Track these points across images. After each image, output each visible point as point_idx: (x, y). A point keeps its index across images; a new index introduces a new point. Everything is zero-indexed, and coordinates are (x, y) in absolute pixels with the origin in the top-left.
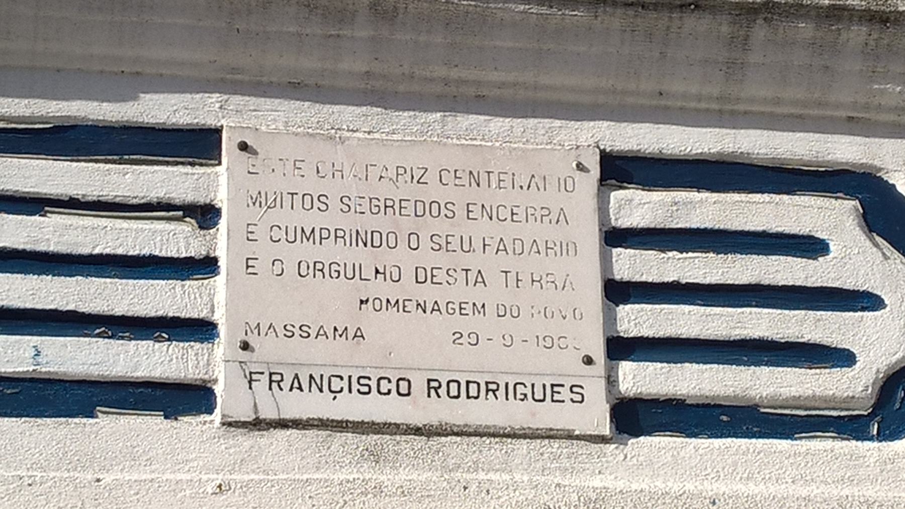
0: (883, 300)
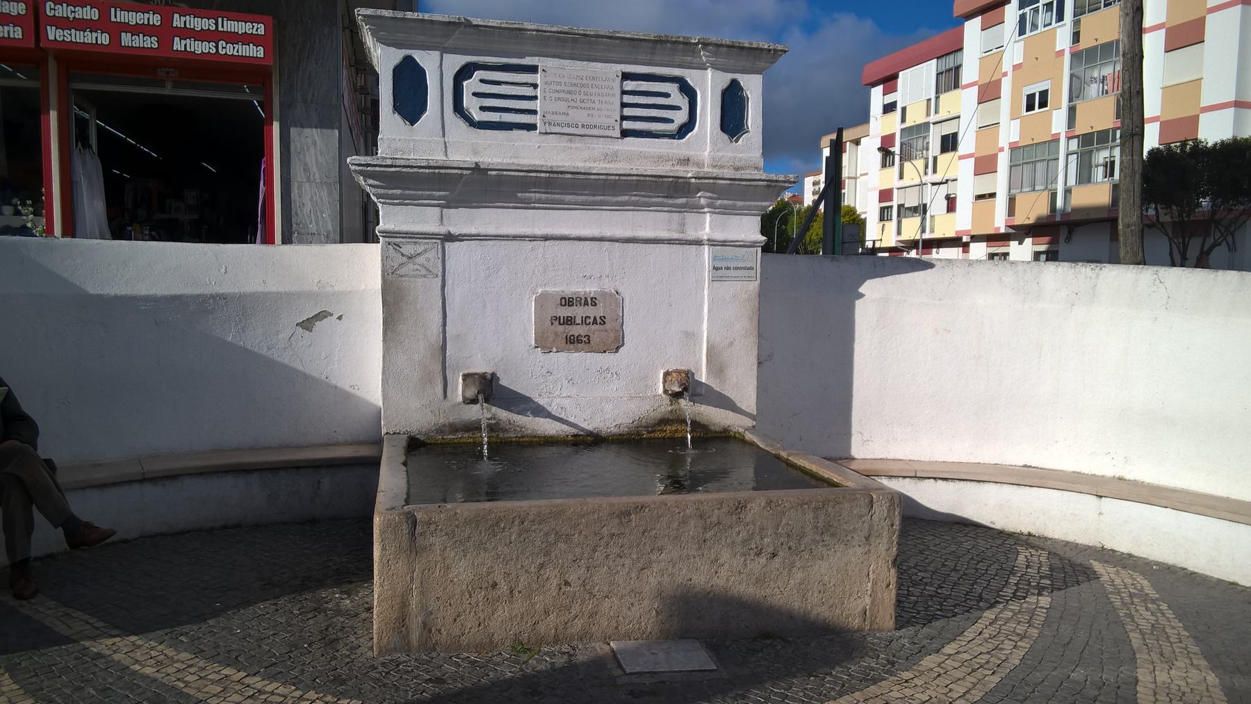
0: (423, 108)
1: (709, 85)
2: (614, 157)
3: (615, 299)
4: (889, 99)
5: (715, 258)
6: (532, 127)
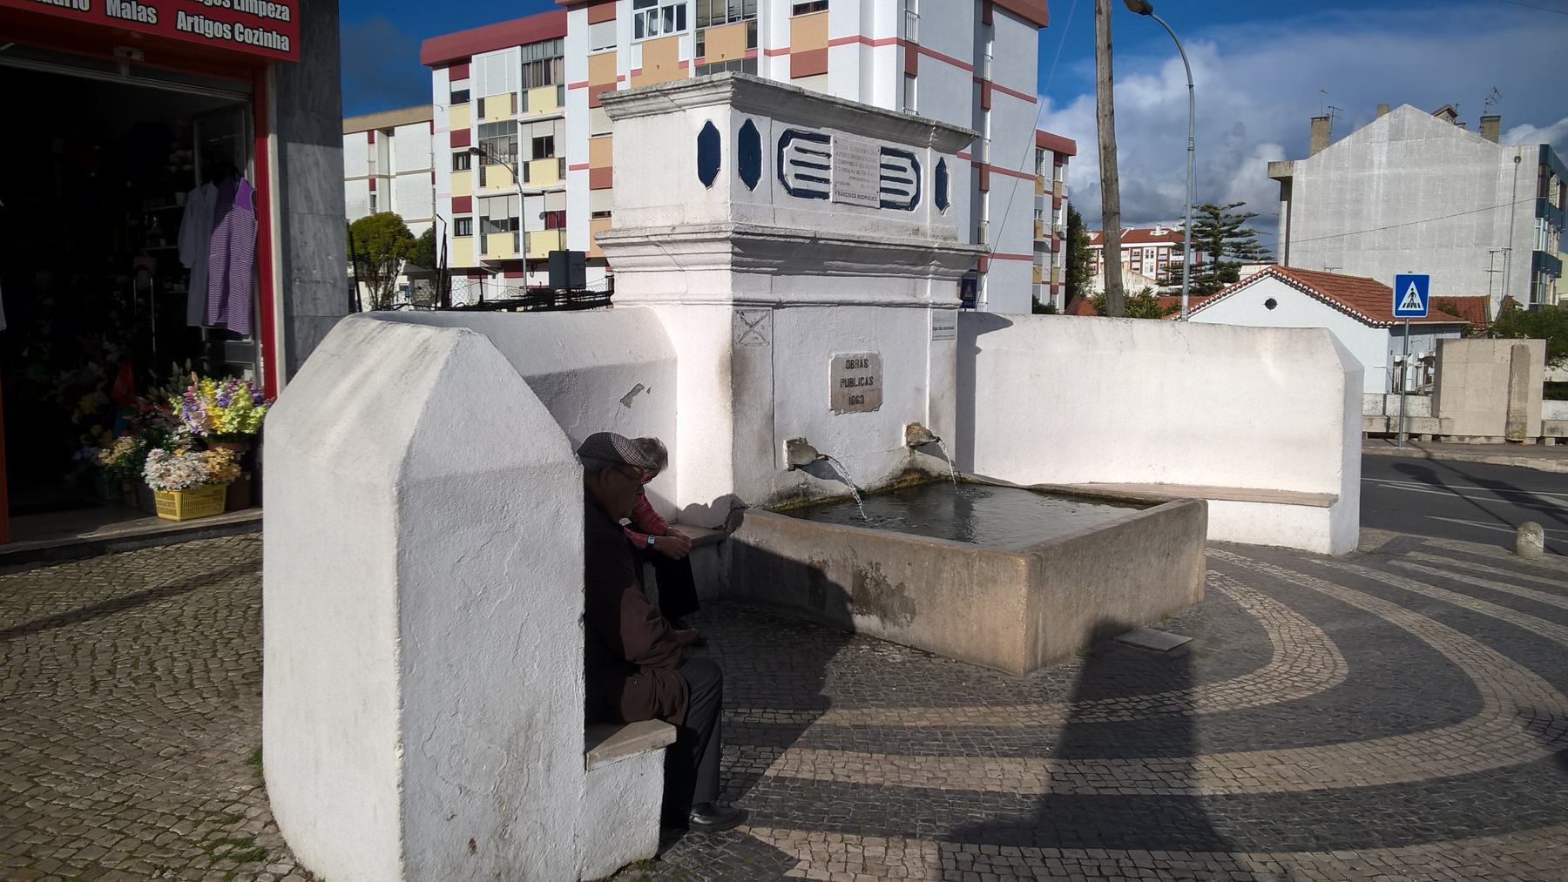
2: (876, 226)
4: (459, 86)
5: (935, 320)
6: (825, 196)
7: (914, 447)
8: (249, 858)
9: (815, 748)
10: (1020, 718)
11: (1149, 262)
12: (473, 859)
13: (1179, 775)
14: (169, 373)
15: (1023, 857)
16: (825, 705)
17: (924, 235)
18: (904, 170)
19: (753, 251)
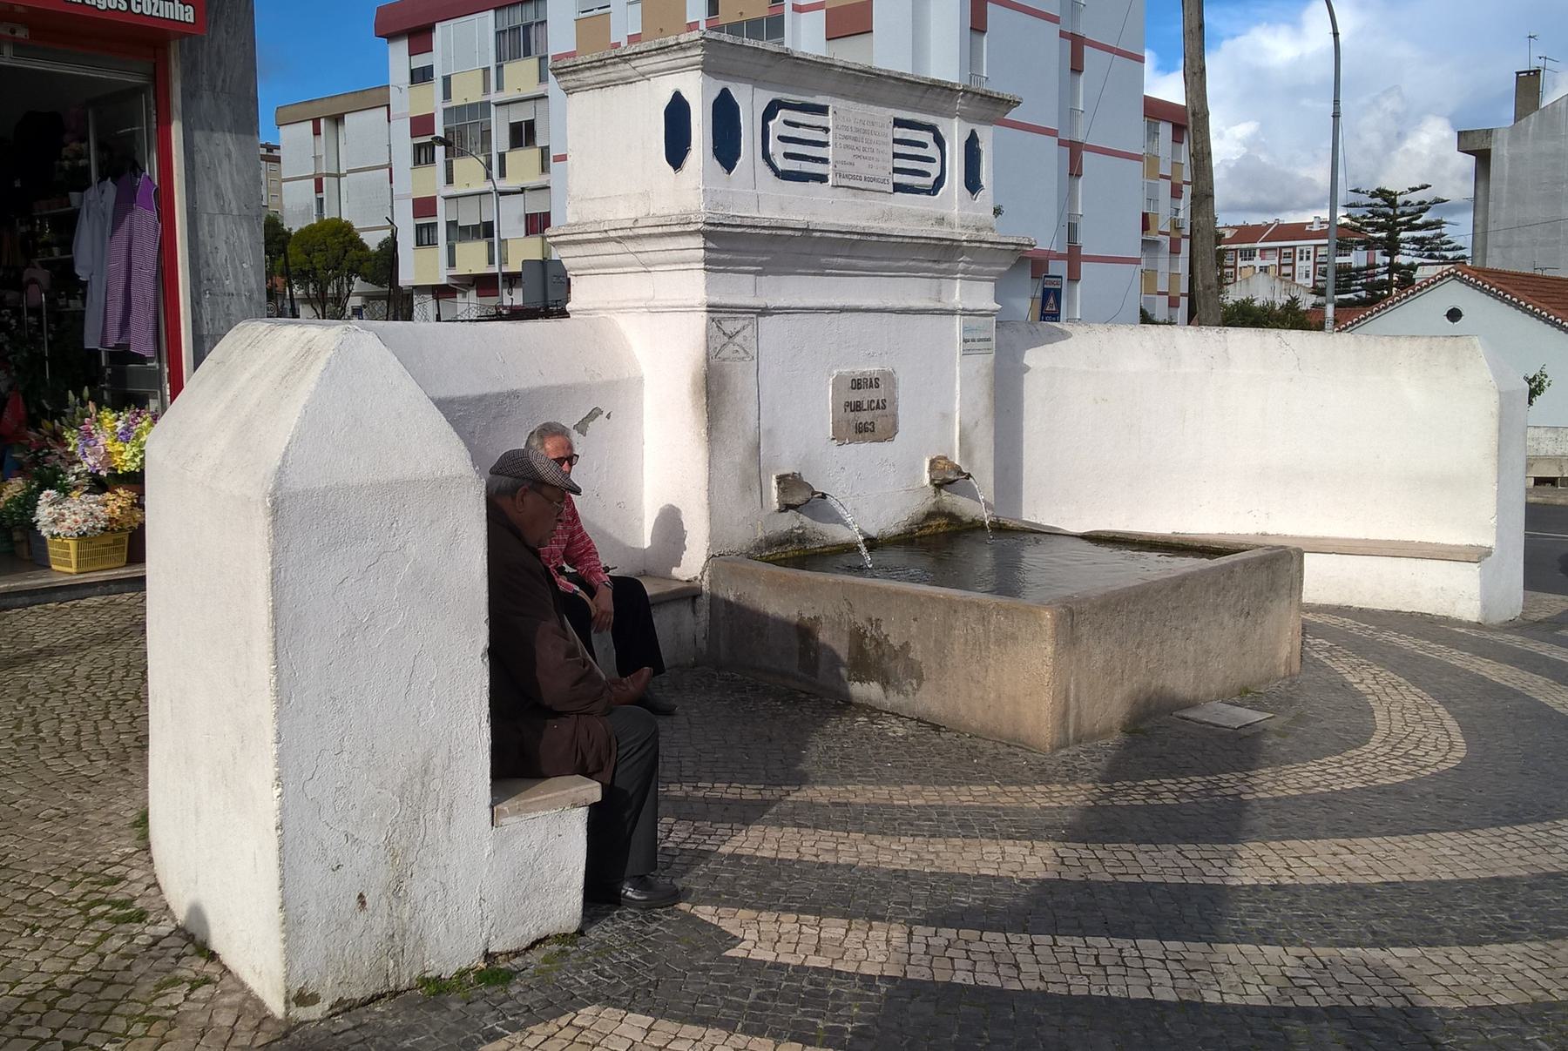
1: (955, 132)
2: (887, 215)
3: (890, 377)
4: (420, 61)
5: (965, 330)
6: (822, 178)
7: (940, 485)
8: (128, 919)
9: (782, 826)
10: (1037, 798)
11: (1304, 266)
12: (362, 916)
13: (1218, 863)
14: (65, 403)
15: (1008, 943)
16: (802, 780)
17: (951, 225)
18: (924, 145)
19: (728, 245)
